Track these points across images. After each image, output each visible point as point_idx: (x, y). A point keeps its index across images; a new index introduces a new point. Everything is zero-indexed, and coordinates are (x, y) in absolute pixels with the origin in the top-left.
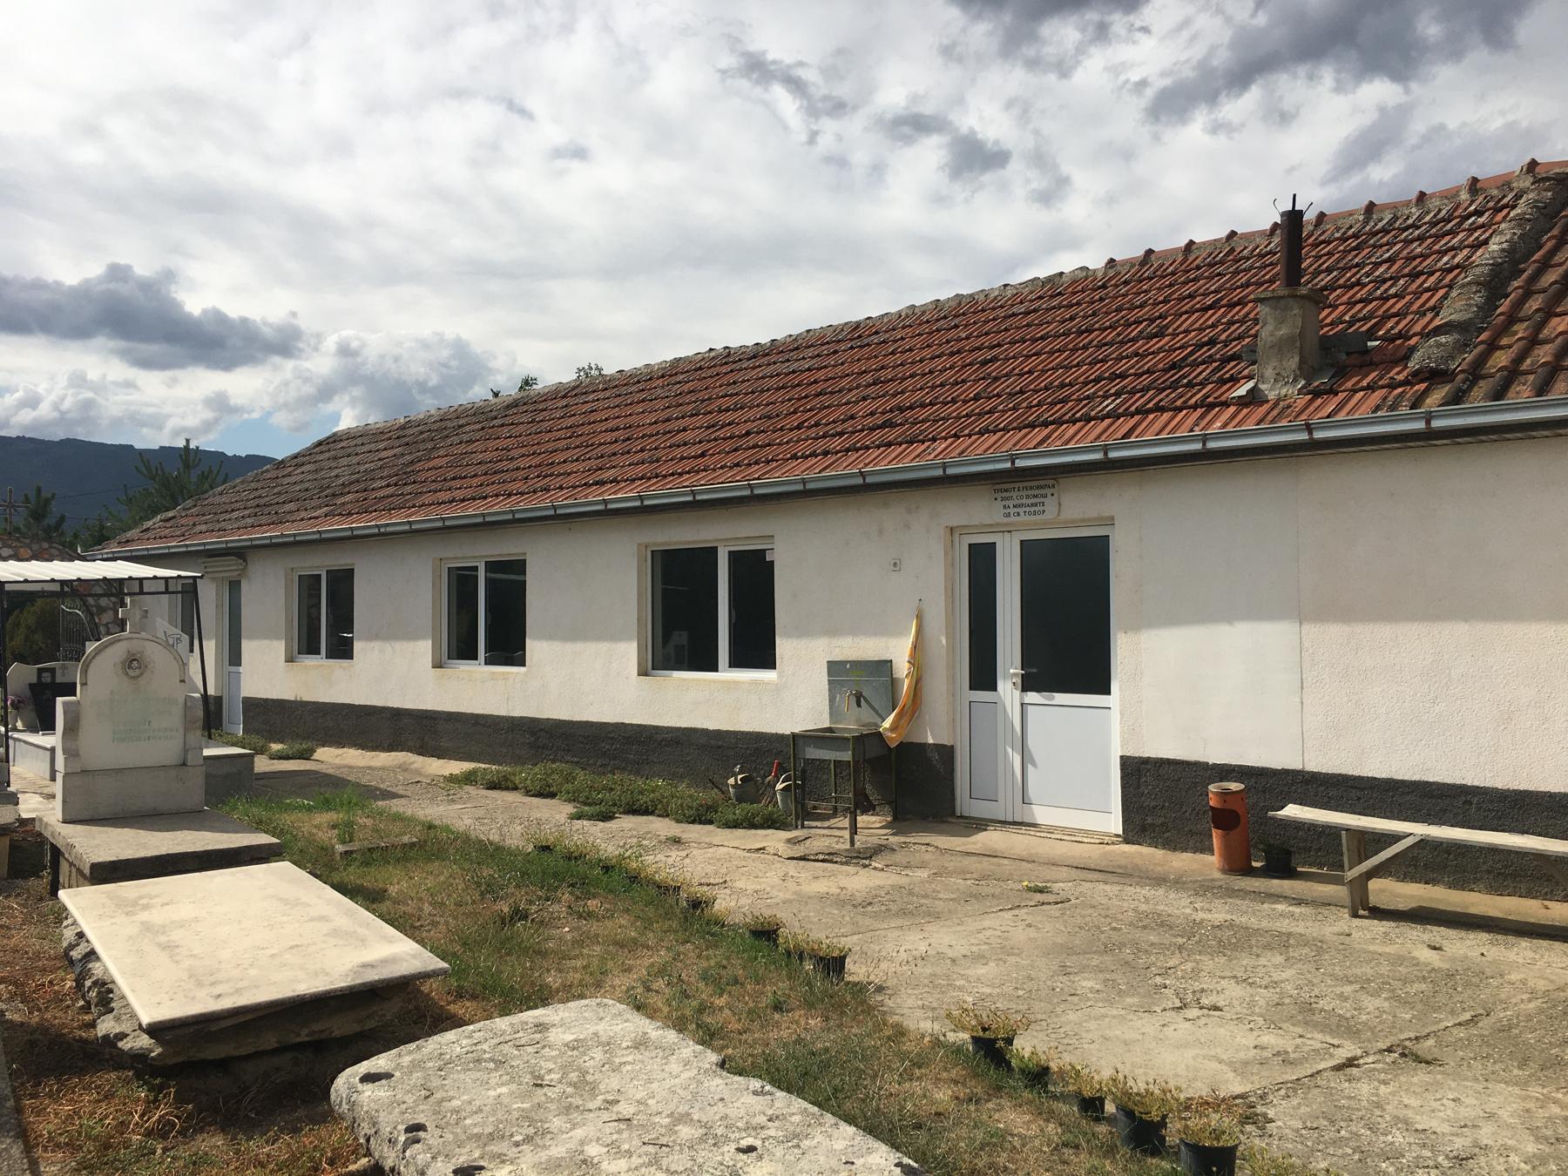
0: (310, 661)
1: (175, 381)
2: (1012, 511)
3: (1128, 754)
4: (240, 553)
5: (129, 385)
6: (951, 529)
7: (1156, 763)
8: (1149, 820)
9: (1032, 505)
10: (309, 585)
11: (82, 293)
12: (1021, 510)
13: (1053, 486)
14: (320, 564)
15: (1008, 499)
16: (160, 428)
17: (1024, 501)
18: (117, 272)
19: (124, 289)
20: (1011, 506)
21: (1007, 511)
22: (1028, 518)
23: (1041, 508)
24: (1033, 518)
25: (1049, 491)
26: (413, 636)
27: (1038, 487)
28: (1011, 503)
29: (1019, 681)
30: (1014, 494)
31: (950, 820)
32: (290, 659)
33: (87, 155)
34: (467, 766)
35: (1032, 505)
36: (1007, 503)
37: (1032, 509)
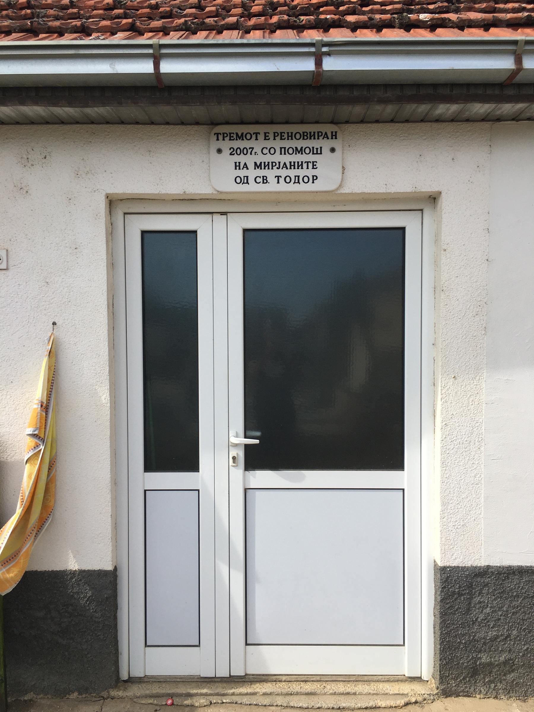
2: (252, 173)
3: (454, 564)
6: (435, 199)
7: (499, 573)
8: (485, 658)
9: (292, 165)
12: (270, 174)
13: (334, 136)
15: (243, 151)
17: (277, 158)
20: (251, 166)
21: (242, 173)
22: (283, 187)
23: (310, 172)
24: (292, 187)
25: (326, 144)
27: (305, 136)
28: (250, 160)
29: (241, 454)
30: (258, 145)
31: (113, 693)
35: (292, 165)
36: (242, 159)
37: (293, 173)
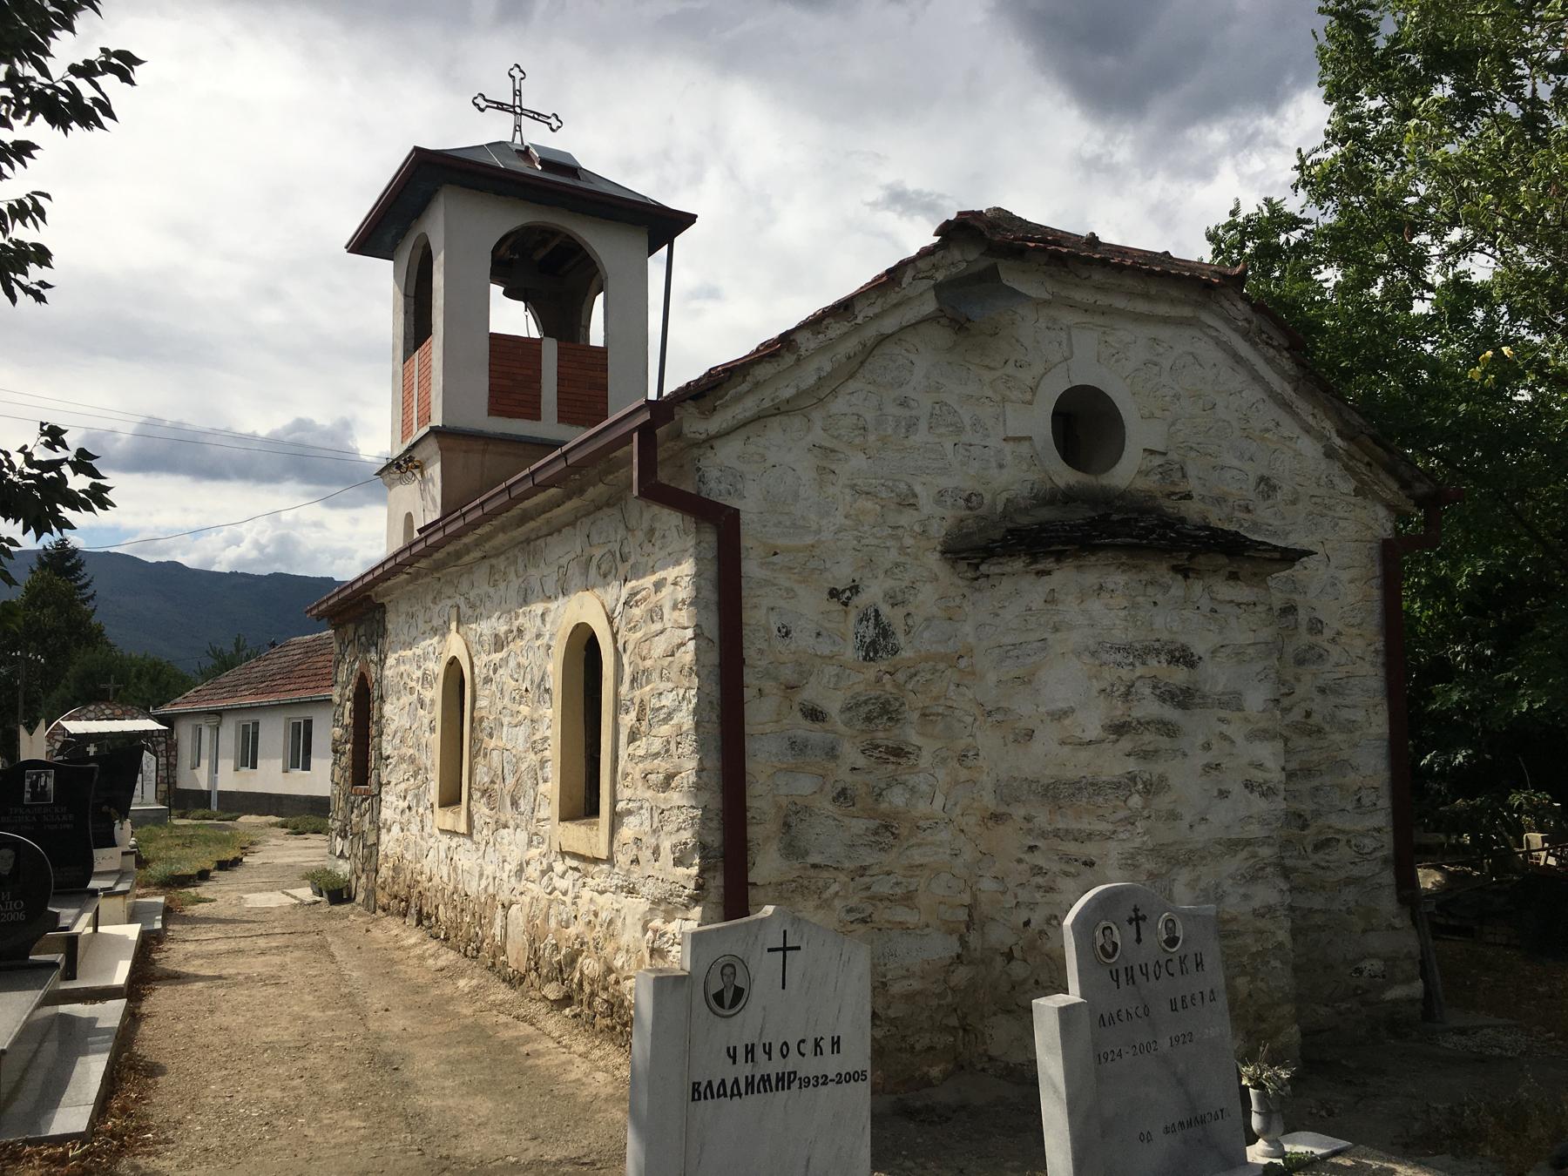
0: (244, 770)
1: (355, 521)
4: (219, 713)
5: (318, 525)
10: (296, 726)
11: (272, 442)
14: (300, 715)
16: (351, 558)
18: (301, 425)
19: (309, 439)
26: (276, 758)
32: (236, 770)
33: (270, 315)
34: (279, 819)
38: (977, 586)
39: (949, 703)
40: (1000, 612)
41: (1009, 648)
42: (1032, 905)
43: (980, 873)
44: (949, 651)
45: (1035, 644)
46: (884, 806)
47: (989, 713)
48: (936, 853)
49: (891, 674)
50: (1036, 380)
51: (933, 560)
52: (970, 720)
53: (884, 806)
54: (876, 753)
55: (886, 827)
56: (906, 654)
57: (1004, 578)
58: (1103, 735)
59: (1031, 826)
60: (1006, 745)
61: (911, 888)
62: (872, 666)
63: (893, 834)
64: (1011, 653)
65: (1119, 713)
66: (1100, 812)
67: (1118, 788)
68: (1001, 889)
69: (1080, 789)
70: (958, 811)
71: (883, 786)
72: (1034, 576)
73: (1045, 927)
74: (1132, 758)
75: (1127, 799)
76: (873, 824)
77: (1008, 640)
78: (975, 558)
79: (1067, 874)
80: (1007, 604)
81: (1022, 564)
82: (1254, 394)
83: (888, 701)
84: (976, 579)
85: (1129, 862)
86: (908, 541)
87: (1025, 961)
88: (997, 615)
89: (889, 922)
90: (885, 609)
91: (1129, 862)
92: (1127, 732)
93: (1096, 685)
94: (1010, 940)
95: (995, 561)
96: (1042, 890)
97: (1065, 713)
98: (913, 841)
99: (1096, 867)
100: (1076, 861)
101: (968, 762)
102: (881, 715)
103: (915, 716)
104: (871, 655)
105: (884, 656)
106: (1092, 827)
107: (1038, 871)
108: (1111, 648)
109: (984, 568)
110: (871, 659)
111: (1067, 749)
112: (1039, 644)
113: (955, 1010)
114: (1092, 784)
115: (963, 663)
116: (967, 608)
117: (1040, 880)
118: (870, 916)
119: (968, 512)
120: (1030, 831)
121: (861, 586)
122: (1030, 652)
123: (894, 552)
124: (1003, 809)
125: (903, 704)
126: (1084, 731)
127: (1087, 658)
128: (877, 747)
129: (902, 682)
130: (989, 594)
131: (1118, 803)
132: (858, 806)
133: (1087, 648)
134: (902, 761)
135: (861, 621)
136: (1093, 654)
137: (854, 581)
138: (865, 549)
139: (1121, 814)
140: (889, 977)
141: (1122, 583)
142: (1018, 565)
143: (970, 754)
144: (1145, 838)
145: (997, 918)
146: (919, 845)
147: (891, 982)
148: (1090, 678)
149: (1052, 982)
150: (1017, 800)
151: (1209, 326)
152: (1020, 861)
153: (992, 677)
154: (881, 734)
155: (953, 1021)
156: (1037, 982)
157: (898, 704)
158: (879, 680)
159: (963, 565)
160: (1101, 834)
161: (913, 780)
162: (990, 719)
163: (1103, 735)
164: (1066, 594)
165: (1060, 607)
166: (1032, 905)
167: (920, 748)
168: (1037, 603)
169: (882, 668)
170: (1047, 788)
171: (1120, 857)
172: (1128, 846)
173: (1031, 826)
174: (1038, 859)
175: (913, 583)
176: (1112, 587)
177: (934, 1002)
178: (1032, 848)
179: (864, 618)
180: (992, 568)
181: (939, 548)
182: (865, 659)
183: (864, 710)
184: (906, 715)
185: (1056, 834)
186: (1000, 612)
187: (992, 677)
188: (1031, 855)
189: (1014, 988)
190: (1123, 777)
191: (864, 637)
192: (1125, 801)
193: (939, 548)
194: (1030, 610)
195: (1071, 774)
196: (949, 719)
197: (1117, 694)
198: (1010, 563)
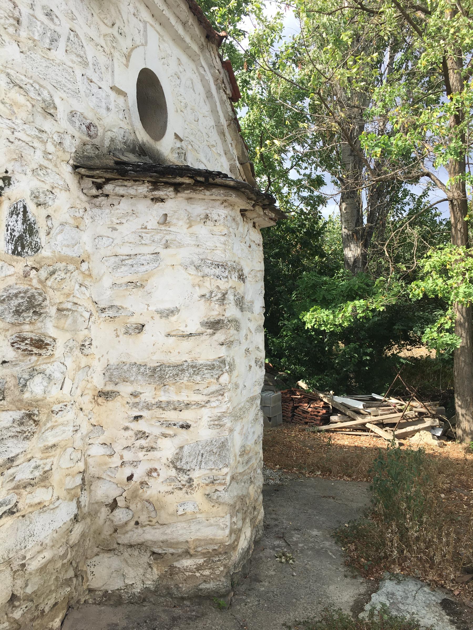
38: (98, 204)
39: (75, 300)
40: (118, 227)
41: (124, 257)
42: (135, 464)
43: (90, 442)
44: (75, 255)
45: (148, 256)
46: (27, 396)
47: (103, 310)
48: (64, 432)
49: (37, 270)
50: (129, 50)
51: (67, 170)
52: (87, 315)
53: (27, 396)
54: (23, 346)
55: (30, 416)
56: (45, 253)
57: (123, 199)
58: (202, 329)
59: (137, 400)
60: (118, 336)
61: (47, 468)
62: (21, 261)
63: (35, 421)
64: (127, 262)
65: (215, 313)
66: (197, 387)
67: (213, 369)
68: (108, 453)
69: (183, 370)
70: (79, 392)
71: (27, 377)
72: (150, 202)
73: (146, 479)
74: (224, 347)
75: (219, 377)
76: (17, 415)
77: (126, 250)
78: (101, 177)
79: (165, 435)
80: (124, 221)
81: (146, 189)
82: (211, 122)
83: (33, 296)
84: (96, 197)
85: (216, 423)
86: (51, 148)
87: (128, 508)
88: (116, 229)
89: (31, 506)
90: (31, 207)
91: (216, 423)
92: (221, 328)
93: (199, 292)
94: (113, 492)
95: (120, 184)
96: (145, 450)
97: (172, 312)
98: (49, 425)
99: (191, 429)
100: (175, 425)
101: (86, 351)
102: (28, 309)
103: (53, 311)
104: (19, 249)
105: (29, 252)
106: (189, 399)
107: (142, 435)
108: (212, 264)
109: (108, 188)
110: (19, 254)
111: (172, 339)
112: (152, 256)
113: (71, 563)
114: (193, 367)
115: (84, 266)
116: (87, 220)
117: (143, 442)
118: (16, 505)
119: (88, 139)
120: (136, 405)
121: (13, 179)
122: (144, 262)
123: (39, 153)
124: (110, 388)
125: (45, 299)
126: (186, 326)
127: (192, 270)
128: (23, 339)
129: (43, 278)
130: (107, 211)
131: (212, 380)
132: (8, 399)
133: (192, 263)
134: (43, 352)
135: (12, 214)
136: (197, 268)
137: (7, 172)
138: (16, 142)
139: (214, 387)
140: (28, 557)
141: (224, 216)
142: (143, 189)
143: (87, 343)
144: (228, 405)
145: (104, 476)
146: (52, 428)
147: (29, 562)
148: (194, 286)
149: (150, 521)
150: (125, 380)
151: (202, 66)
152: (126, 429)
153: (107, 282)
154: (27, 327)
155: (71, 573)
156: (137, 523)
157: (41, 299)
158: (26, 275)
159: (88, 182)
160: (197, 404)
161: (49, 369)
162: (103, 315)
163: (202, 329)
164: (178, 219)
165: (172, 229)
166: (135, 464)
167: (54, 340)
168: (152, 223)
169: (29, 263)
170: (154, 370)
171: (209, 419)
172: (217, 412)
173: (137, 400)
174: (141, 426)
175: (53, 188)
176: (216, 217)
177: (59, 565)
178: (137, 418)
179: (14, 212)
180: (117, 188)
181: (71, 162)
182: (13, 253)
183: (14, 302)
184: (47, 310)
185: (159, 405)
186: (118, 227)
187: (107, 282)
188: (135, 423)
189: (116, 531)
190: (214, 360)
191: (14, 230)
192: (218, 379)
193: (71, 162)
194: (146, 228)
195: (174, 359)
196: (75, 313)
197: (214, 299)
198: (135, 187)
